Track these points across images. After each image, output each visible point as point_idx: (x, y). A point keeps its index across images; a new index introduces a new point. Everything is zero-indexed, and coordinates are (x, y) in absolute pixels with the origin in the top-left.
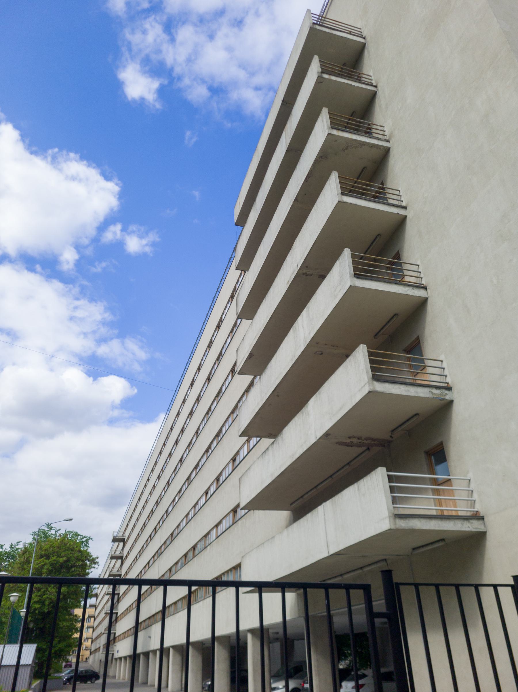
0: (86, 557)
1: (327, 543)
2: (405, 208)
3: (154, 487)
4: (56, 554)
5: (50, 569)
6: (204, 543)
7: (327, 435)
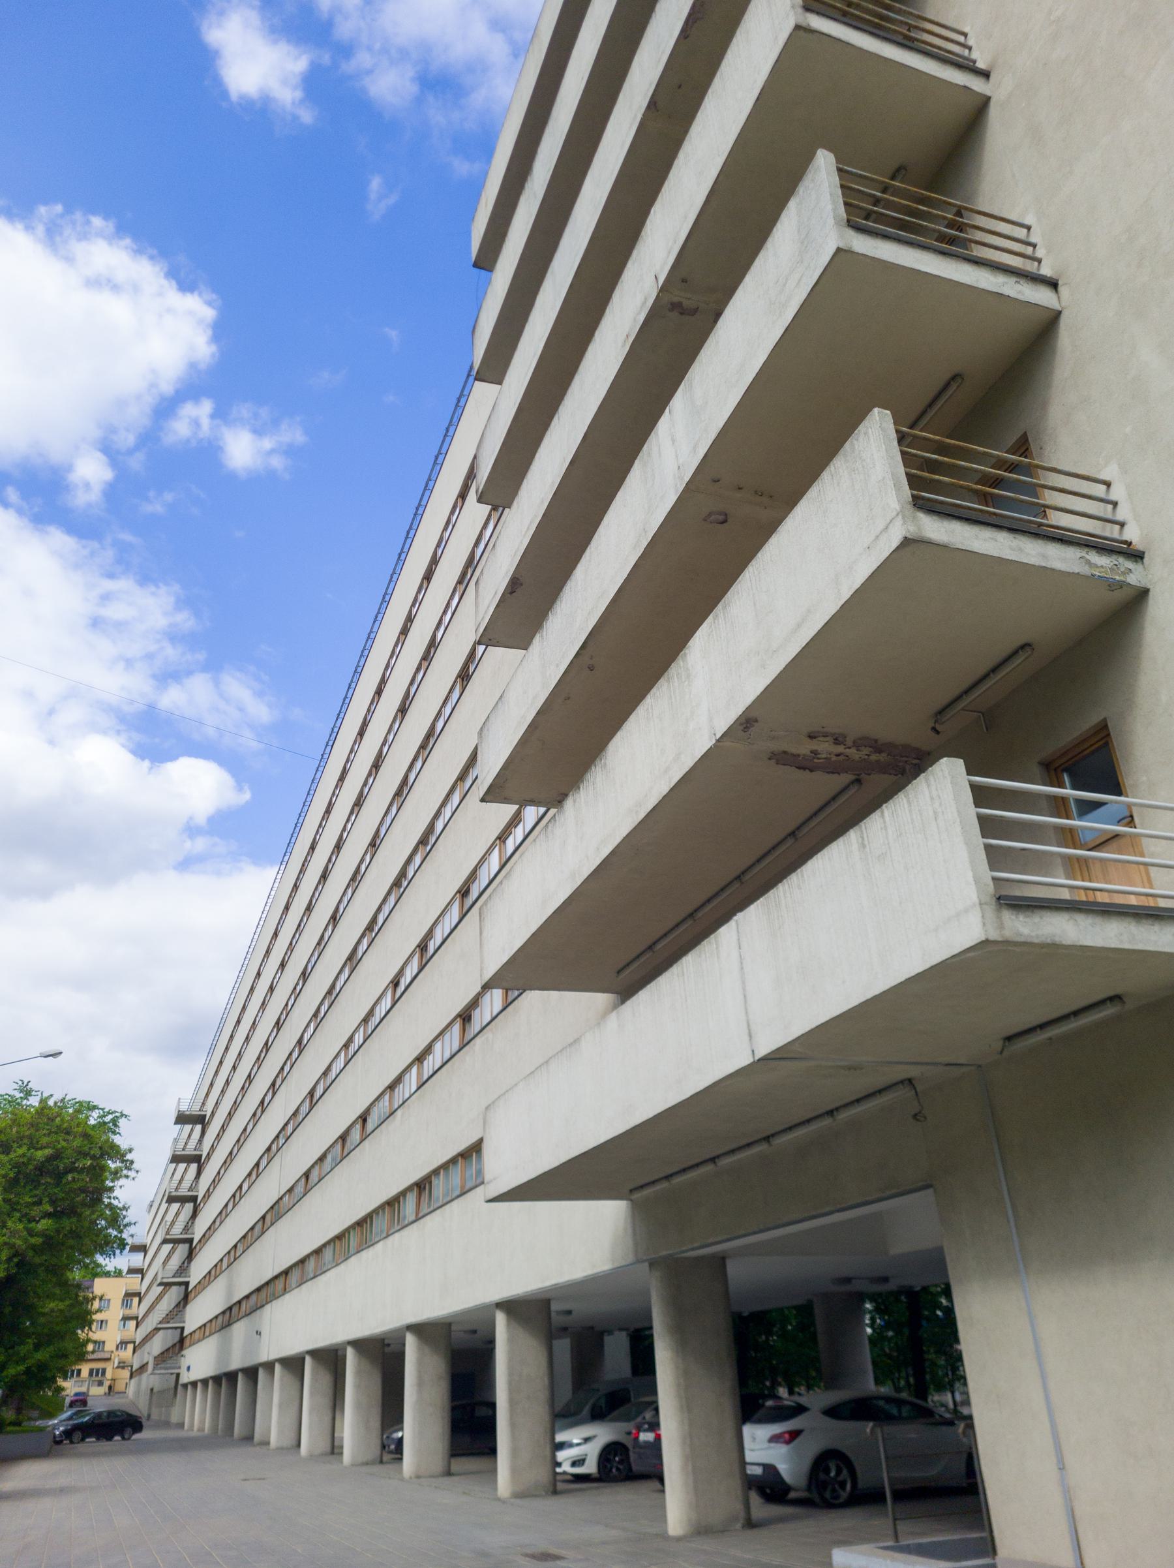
0: (101, 1148)
1: (749, 1025)
2: (985, 75)
3: (271, 989)
4: (26, 1141)
5: (12, 1175)
6: (387, 1104)
7: (746, 722)
